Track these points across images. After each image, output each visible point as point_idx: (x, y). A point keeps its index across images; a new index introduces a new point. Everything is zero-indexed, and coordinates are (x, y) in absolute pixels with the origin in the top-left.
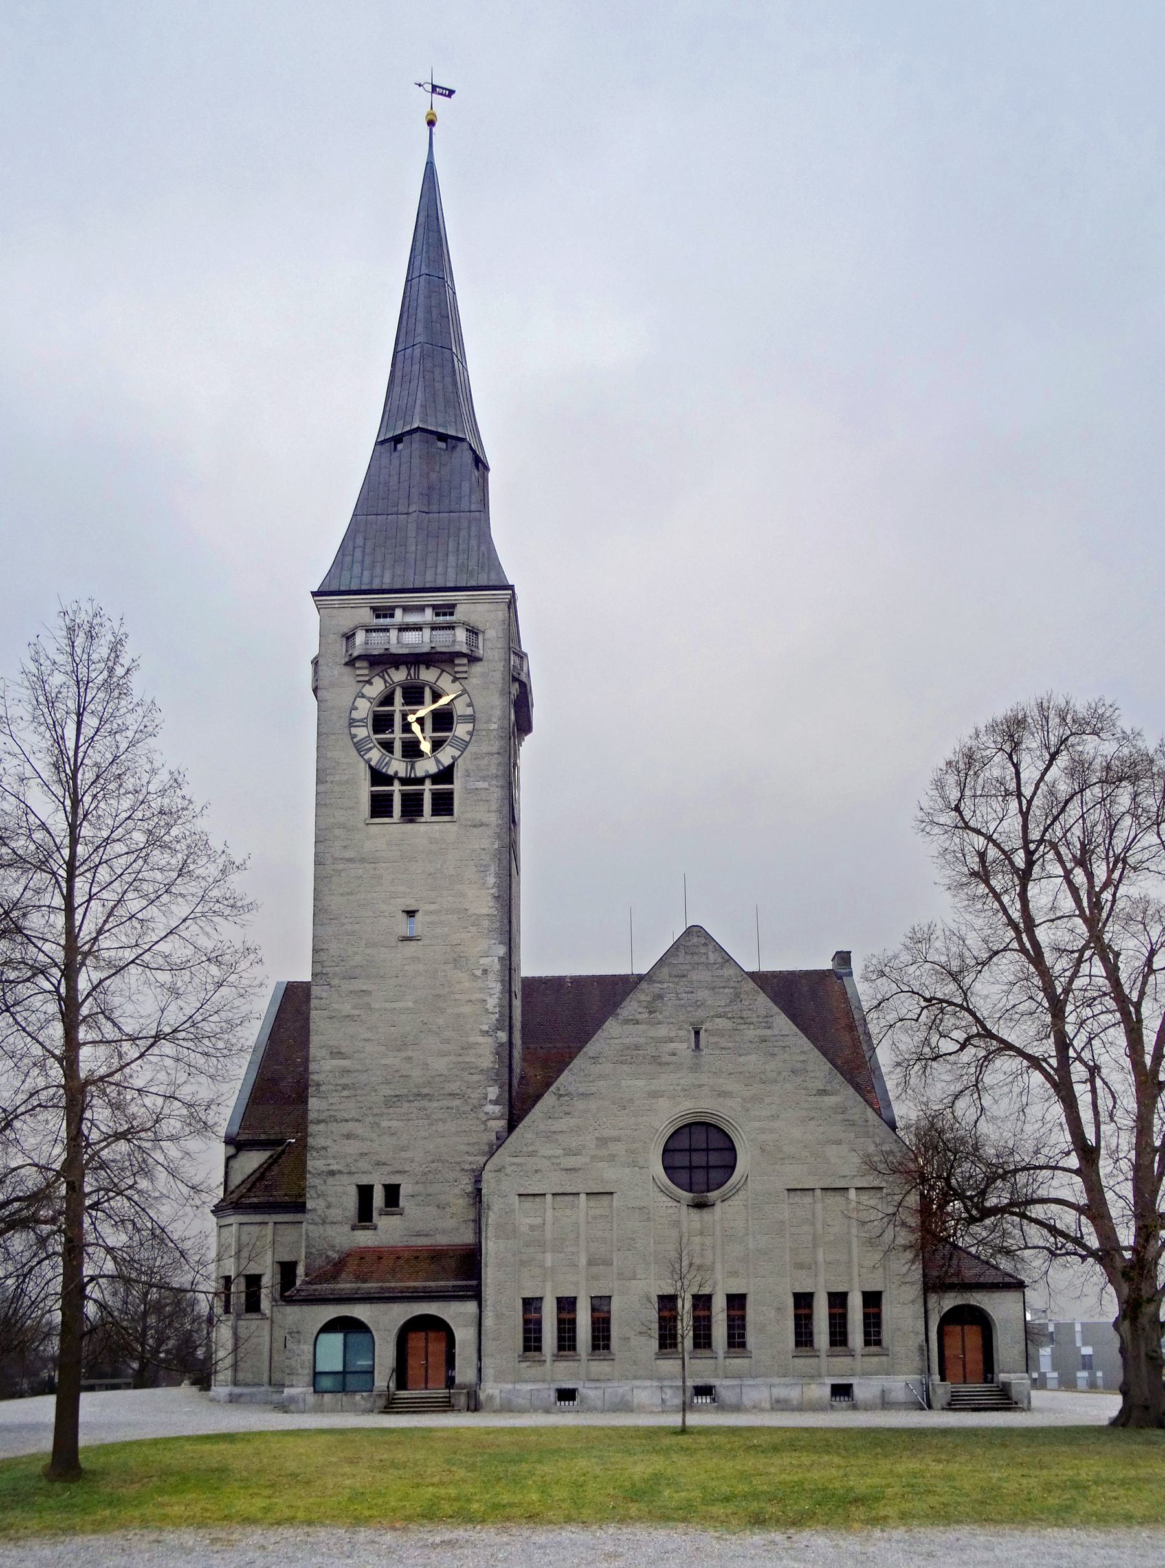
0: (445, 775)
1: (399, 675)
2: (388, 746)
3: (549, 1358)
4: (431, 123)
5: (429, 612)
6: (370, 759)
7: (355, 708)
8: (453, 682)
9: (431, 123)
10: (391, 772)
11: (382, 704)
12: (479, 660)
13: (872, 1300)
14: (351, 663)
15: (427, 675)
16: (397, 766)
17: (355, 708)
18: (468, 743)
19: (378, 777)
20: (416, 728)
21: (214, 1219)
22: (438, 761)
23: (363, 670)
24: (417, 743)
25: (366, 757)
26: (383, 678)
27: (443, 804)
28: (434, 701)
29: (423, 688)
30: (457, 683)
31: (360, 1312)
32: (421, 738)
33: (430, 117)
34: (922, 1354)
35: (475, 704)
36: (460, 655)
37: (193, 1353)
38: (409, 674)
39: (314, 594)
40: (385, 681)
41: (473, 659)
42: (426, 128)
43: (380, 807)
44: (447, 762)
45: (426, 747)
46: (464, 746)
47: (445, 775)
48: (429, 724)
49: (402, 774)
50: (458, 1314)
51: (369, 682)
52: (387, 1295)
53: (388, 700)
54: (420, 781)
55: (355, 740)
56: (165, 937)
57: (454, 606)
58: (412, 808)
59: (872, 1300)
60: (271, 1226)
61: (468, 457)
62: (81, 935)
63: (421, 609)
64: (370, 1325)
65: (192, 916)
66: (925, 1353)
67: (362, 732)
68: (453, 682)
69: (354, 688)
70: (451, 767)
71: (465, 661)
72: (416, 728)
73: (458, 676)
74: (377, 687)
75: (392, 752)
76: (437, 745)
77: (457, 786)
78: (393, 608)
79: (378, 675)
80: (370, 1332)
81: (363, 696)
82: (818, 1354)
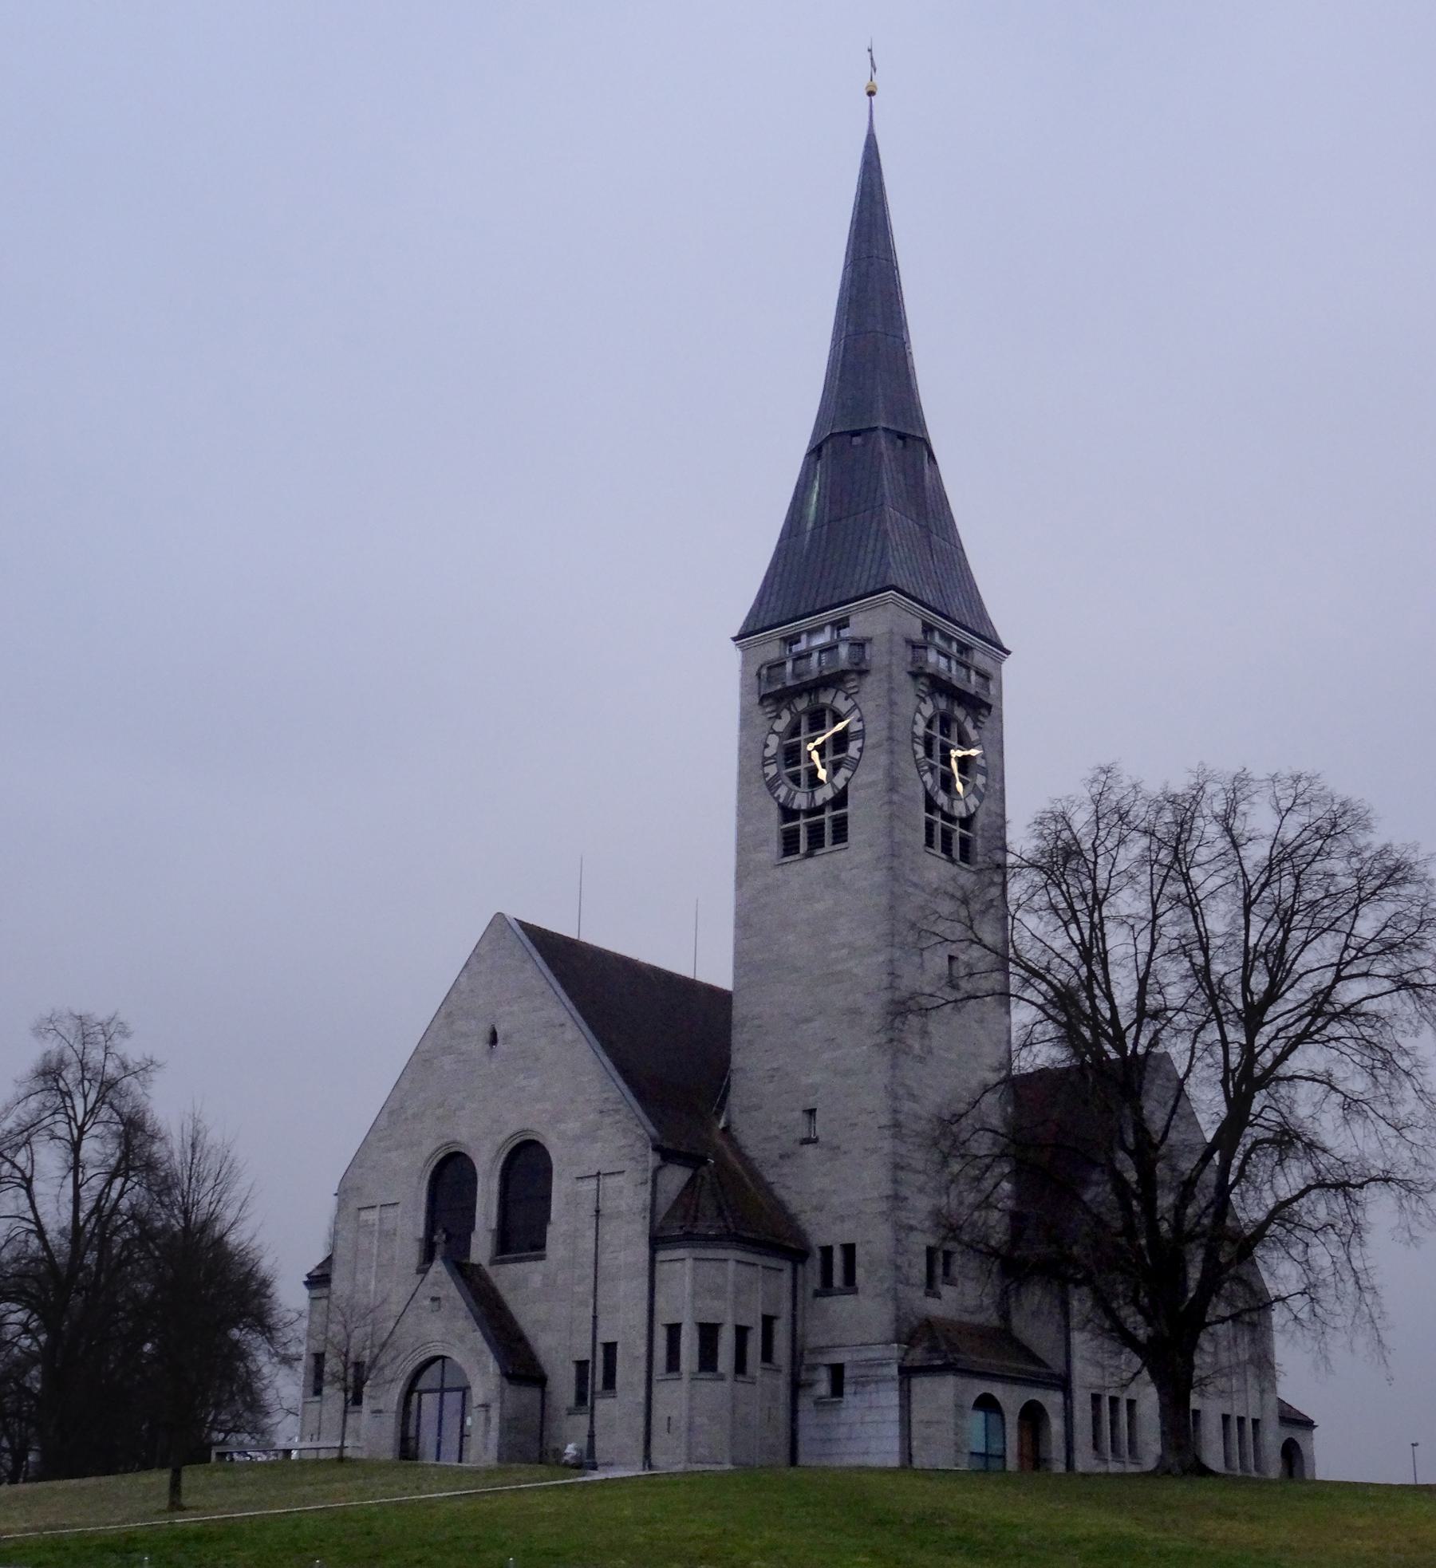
0: (840, 799)
1: (802, 704)
2: (795, 779)
3: (686, 1376)
7: (766, 746)
8: (846, 699)
9: (871, 94)
10: (795, 807)
14: (915, 675)
15: (825, 698)
16: (801, 801)
17: (766, 746)
18: (859, 760)
19: (788, 813)
22: (834, 786)
24: (816, 770)
26: (789, 709)
27: (841, 832)
28: (835, 724)
30: (850, 700)
31: (998, 1391)
32: (819, 766)
37: (111, 1252)
38: (810, 700)
39: (735, 639)
40: (791, 713)
41: (863, 673)
42: (869, 54)
43: (789, 843)
45: (822, 774)
46: (855, 765)
47: (840, 799)
50: (1052, 1401)
51: (778, 717)
53: (795, 731)
54: (820, 810)
55: (767, 779)
57: (847, 618)
58: (816, 839)
60: (689, 1263)
63: (820, 629)
65: (1106, 789)
72: (815, 755)
75: (798, 785)
78: (799, 634)
80: (1002, 1415)
82: (1140, 1461)
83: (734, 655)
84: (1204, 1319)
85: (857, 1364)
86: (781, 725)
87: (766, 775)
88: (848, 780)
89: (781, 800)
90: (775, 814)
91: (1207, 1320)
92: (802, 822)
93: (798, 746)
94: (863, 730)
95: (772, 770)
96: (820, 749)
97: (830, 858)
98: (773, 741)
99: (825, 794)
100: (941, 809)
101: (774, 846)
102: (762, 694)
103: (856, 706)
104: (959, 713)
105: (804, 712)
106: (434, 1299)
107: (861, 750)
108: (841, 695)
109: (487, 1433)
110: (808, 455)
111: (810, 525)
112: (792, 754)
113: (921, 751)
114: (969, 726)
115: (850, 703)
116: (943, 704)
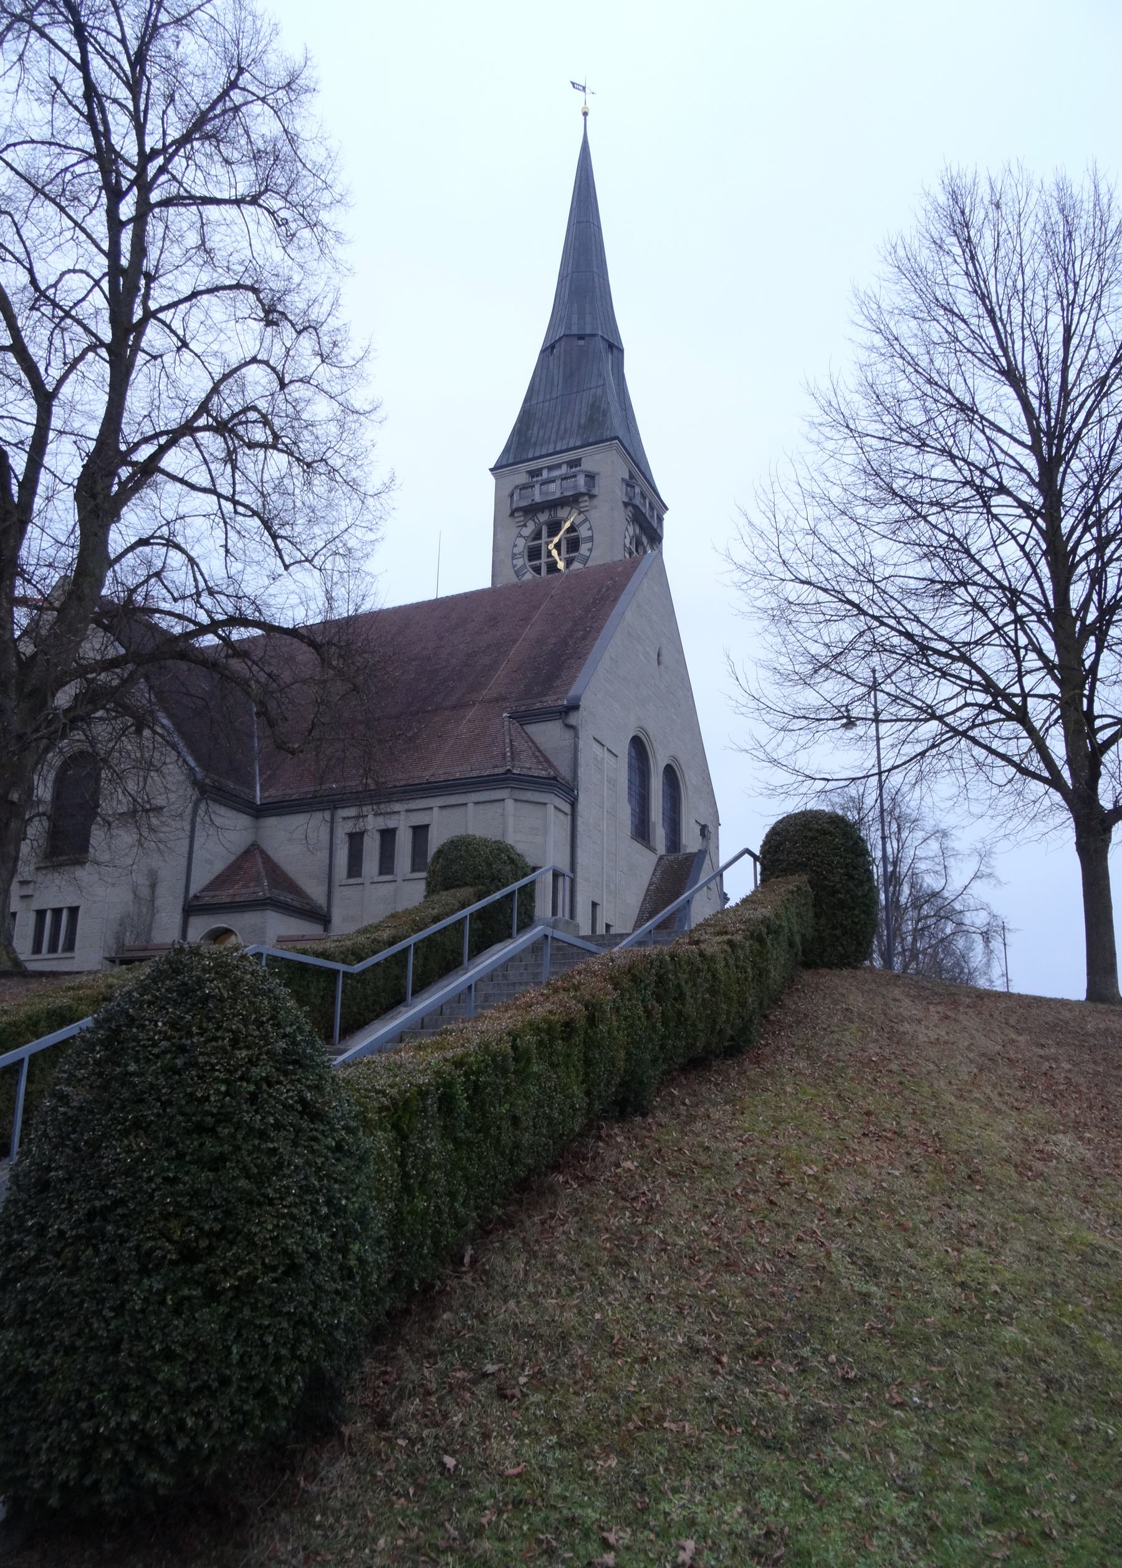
1: (543, 517)
4: (585, 114)
5: (564, 467)
9: (585, 114)
11: (535, 539)
13: (355, 867)
14: (626, 505)
20: (555, 553)
23: (520, 517)
24: (556, 563)
34: (671, 774)
36: (583, 494)
41: (592, 497)
45: (561, 565)
51: (525, 525)
53: (537, 536)
56: (12, 168)
59: (355, 867)
61: (602, 346)
62: (1065, 490)
63: (559, 466)
67: (519, 562)
69: (515, 531)
72: (555, 553)
74: (531, 527)
76: (569, 563)
83: (491, 481)
84: (107, 554)
86: (527, 531)
91: (112, 556)
93: (539, 547)
95: (519, 562)
96: (558, 546)
98: (521, 543)
102: (514, 506)
103: (586, 520)
105: (546, 523)
107: (590, 550)
109: (317, 955)
110: (543, 351)
112: (534, 553)
115: (582, 517)
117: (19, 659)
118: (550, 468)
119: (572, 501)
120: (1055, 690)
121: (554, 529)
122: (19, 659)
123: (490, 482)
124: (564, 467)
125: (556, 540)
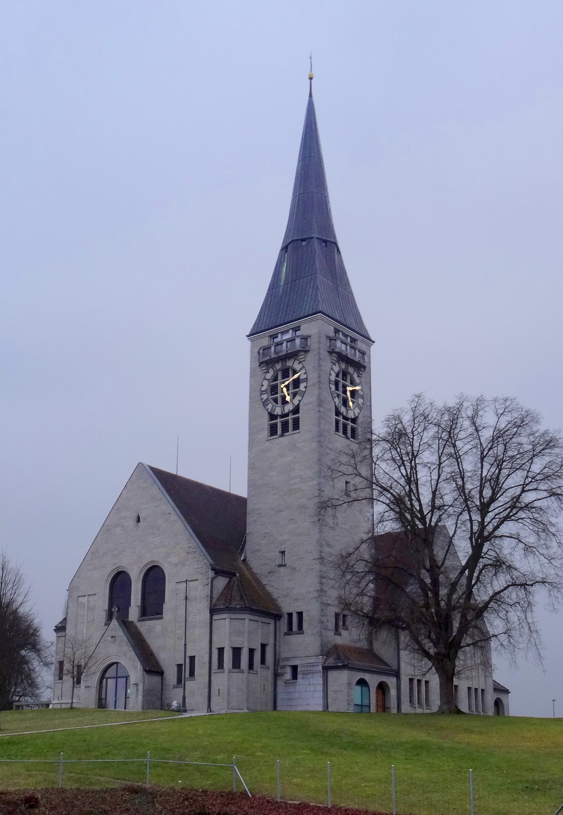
0: (296, 410)
1: (278, 366)
2: (276, 401)
4: (311, 79)
6: (268, 409)
7: (262, 386)
9: (311, 79)
10: (275, 413)
12: (308, 351)
14: (330, 353)
15: (289, 363)
16: (278, 411)
18: (305, 392)
19: (272, 417)
21: (55, 634)
22: (293, 404)
24: (285, 397)
25: (267, 408)
27: (296, 425)
29: (289, 369)
31: (367, 677)
32: (287, 395)
33: (310, 76)
35: (307, 373)
36: (299, 351)
39: (248, 336)
40: (274, 370)
41: (307, 352)
42: (309, 81)
43: (273, 431)
44: (296, 403)
45: (288, 398)
47: (296, 410)
48: (291, 387)
49: (280, 413)
52: (374, 670)
53: (275, 379)
54: (287, 415)
55: (263, 401)
58: (285, 428)
63: (287, 331)
64: (369, 684)
66: (326, 685)
68: (299, 364)
70: (299, 404)
71: (302, 353)
72: (285, 390)
73: (301, 360)
74: (271, 372)
75: (277, 403)
77: (301, 415)
78: (278, 334)
79: (271, 367)
81: (266, 379)
85: (303, 666)
86: (269, 376)
87: (262, 399)
88: (300, 401)
89: (269, 411)
90: (266, 417)
92: (279, 420)
94: (307, 378)
95: (265, 397)
96: (287, 387)
97: (291, 437)
98: (266, 383)
99: (289, 408)
100: (342, 414)
101: (266, 432)
102: (260, 361)
103: (303, 367)
104: (351, 370)
106: (112, 637)
107: (306, 387)
108: (297, 362)
110: (282, 250)
111: (282, 284)
112: (274, 389)
113: (333, 388)
114: (355, 376)
115: (301, 365)
116: (343, 366)
117: (326, 660)
118: (283, 333)
119: (294, 355)
120: (480, 520)
121: (286, 375)
122: (326, 660)
123: (247, 344)
124: (291, 331)
125: (286, 383)
